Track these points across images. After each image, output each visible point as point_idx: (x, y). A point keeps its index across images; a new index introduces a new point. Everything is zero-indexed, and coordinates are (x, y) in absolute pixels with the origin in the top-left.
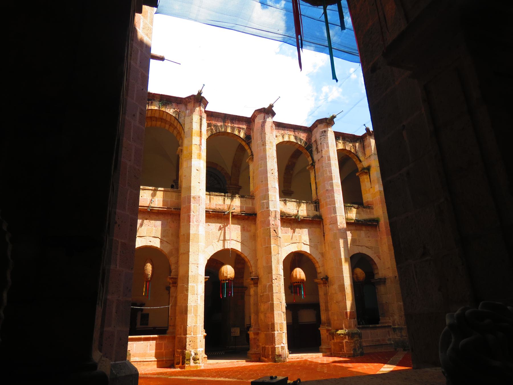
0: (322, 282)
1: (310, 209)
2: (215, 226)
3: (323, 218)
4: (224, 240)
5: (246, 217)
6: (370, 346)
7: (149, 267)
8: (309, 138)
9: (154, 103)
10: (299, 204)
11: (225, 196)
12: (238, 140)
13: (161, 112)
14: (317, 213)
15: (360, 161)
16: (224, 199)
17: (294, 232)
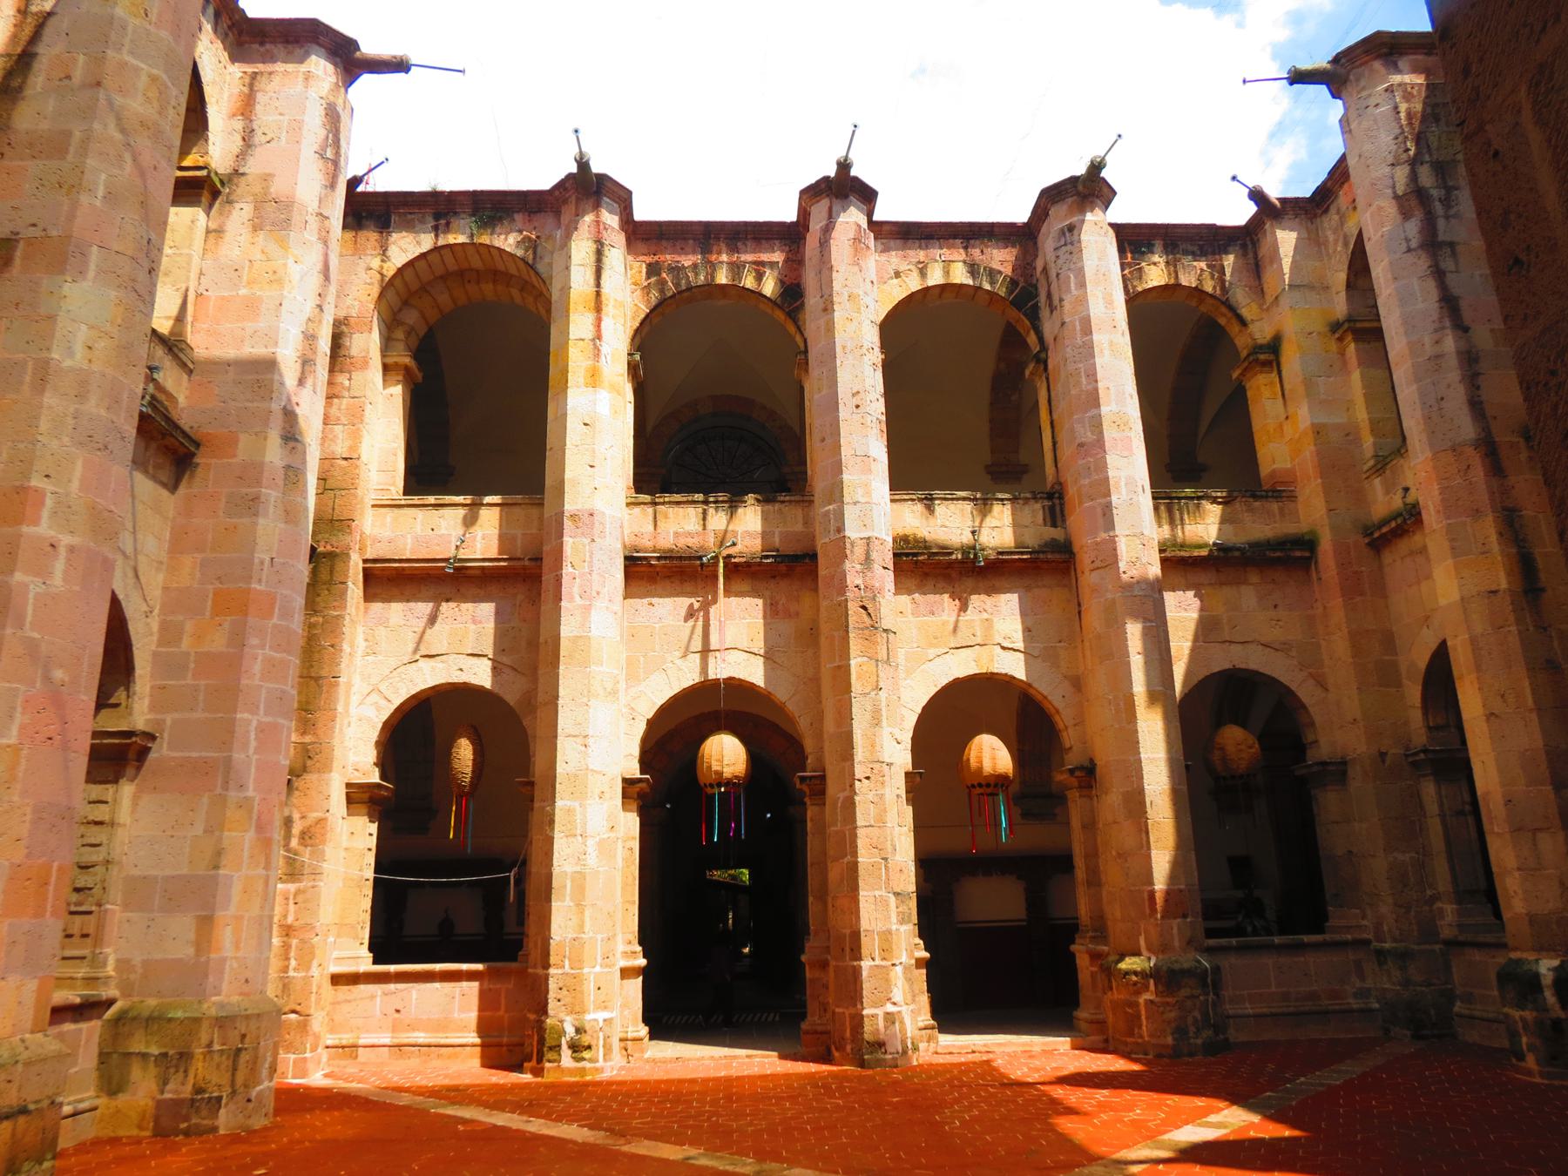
0: (1074, 782)
1: (1027, 520)
2: (668, 610)
3: (1075, 550)
4: (706, 651)
5: (783, 568)
6: (1273, 1015)
7: (464, 752)
8: (1025, 265)
9: (455, 223)
10: (984, 505)
11: (706, 502)
12: (762, 306)
13: (482, 250)
14: (1056, 533)
15: (1243, 322)
16: (705, 512)
17: (964, 608)
